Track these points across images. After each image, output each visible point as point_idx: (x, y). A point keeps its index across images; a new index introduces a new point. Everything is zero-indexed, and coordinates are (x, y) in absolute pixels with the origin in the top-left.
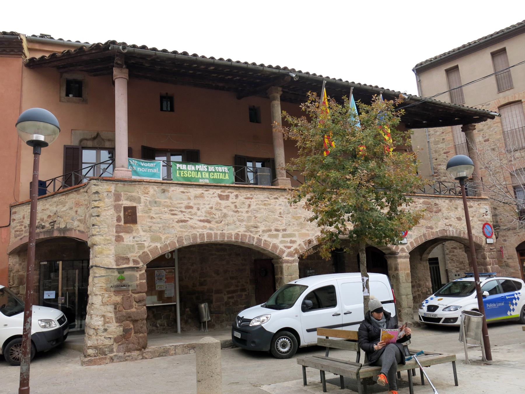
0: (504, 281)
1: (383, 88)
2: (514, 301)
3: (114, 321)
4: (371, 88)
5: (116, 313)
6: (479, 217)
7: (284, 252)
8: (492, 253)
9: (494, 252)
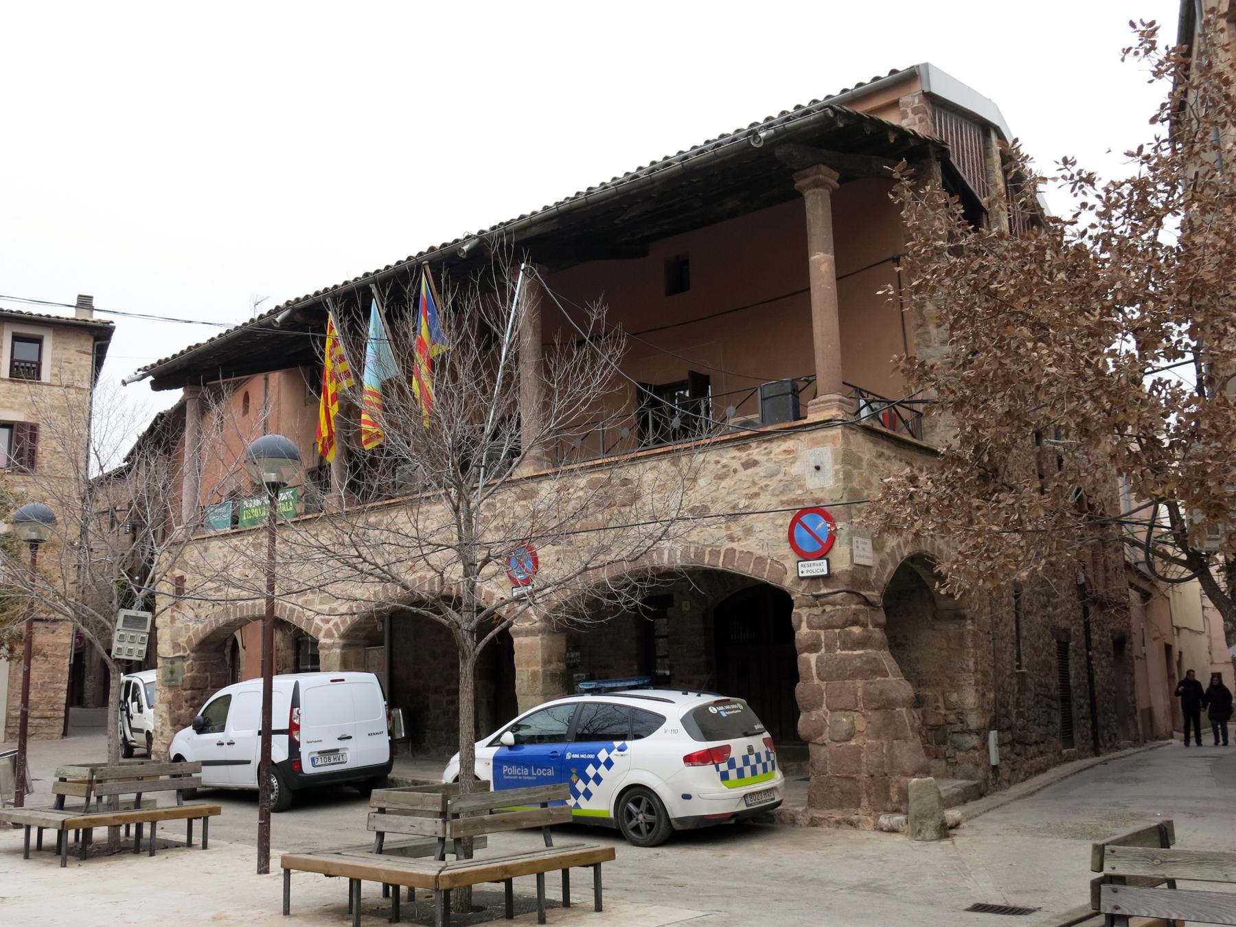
0: (571, 709)
1: (421, 254)
2: (590, 770)
3: (169, 723)
4: (239, 331)
5: (170, 713)
6: (782, 493)
7: (319, 630)
8: (829, 608)
9: (834, 604)
